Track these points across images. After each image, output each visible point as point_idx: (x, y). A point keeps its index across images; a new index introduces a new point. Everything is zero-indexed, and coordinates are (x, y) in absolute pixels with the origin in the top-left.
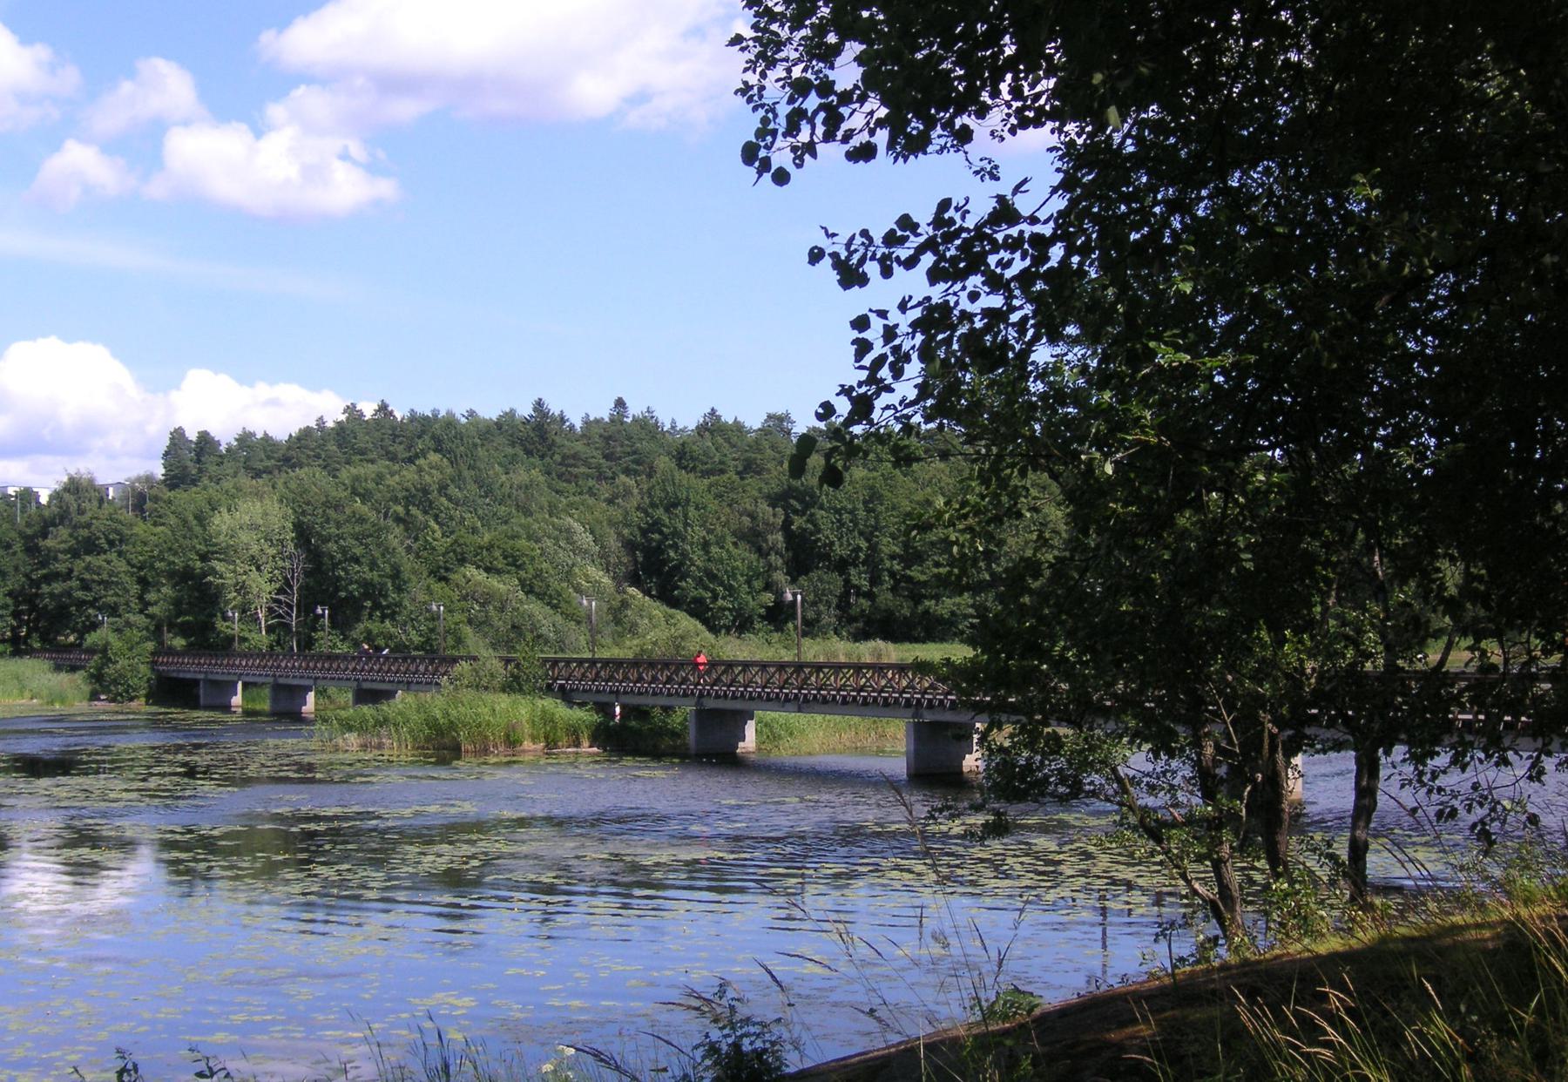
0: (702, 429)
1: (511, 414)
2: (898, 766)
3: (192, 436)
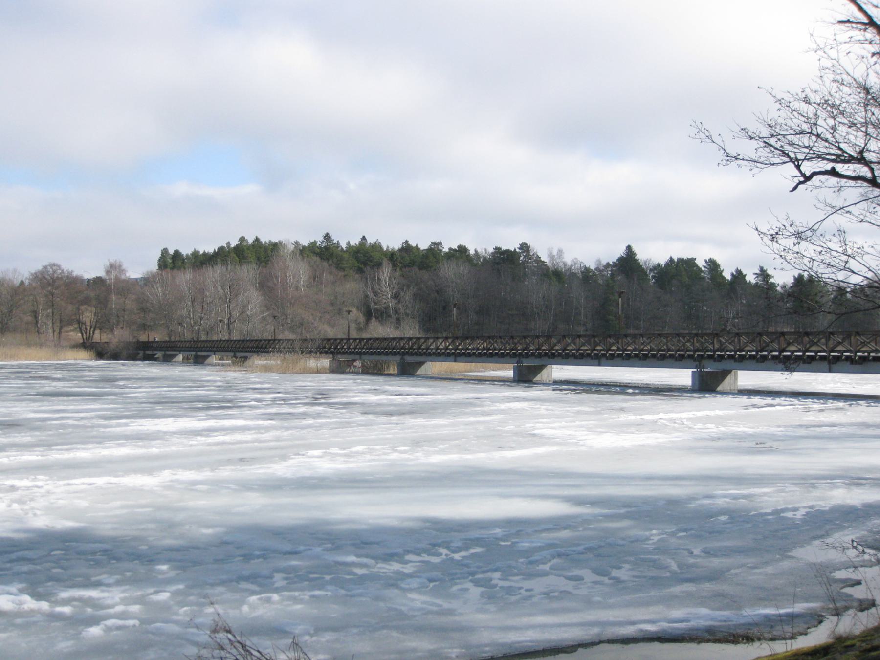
0: (402, 250)
1: (315, 243)
2: (396, 372)
3: (171, 252)
